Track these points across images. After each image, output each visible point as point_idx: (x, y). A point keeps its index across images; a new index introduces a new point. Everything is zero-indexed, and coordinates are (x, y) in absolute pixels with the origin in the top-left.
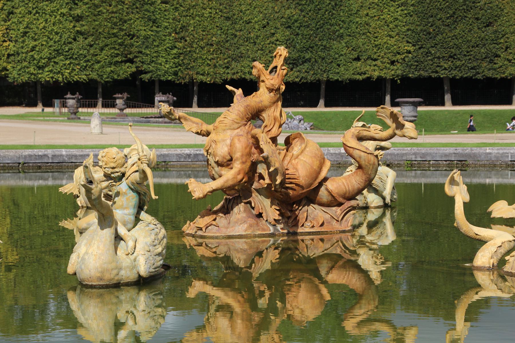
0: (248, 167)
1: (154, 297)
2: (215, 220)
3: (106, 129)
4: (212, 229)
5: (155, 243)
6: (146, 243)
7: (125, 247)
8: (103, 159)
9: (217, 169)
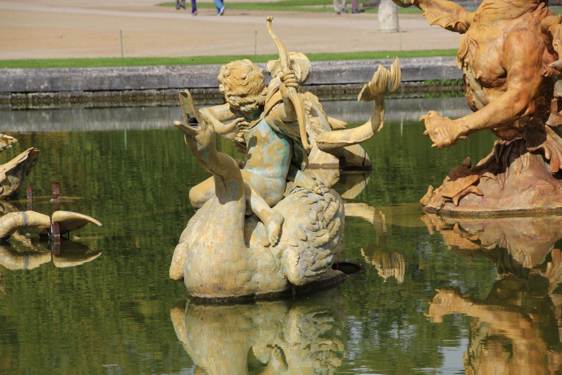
0: (535, 86)
1: (315, 320)
2: (476, 184)
3: (404, 23)
4: (470, 201)
5: (316, 227)
6: (300, 227)
7: (265, 232)
9: (480, 92)
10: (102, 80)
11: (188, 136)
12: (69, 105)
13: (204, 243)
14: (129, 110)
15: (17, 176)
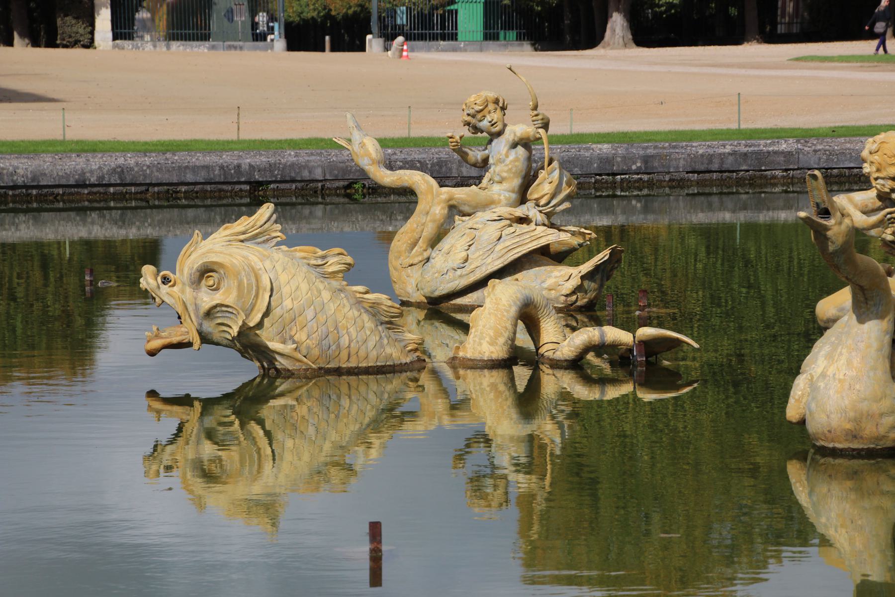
8: (871, 158)
10: (710, 158)
11: (816, 232)
12: (667, 190)
13: (834, 375)
14: (744, 197)
15: (594, 281)
